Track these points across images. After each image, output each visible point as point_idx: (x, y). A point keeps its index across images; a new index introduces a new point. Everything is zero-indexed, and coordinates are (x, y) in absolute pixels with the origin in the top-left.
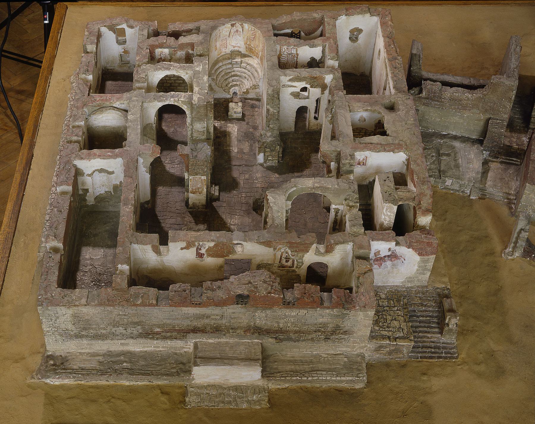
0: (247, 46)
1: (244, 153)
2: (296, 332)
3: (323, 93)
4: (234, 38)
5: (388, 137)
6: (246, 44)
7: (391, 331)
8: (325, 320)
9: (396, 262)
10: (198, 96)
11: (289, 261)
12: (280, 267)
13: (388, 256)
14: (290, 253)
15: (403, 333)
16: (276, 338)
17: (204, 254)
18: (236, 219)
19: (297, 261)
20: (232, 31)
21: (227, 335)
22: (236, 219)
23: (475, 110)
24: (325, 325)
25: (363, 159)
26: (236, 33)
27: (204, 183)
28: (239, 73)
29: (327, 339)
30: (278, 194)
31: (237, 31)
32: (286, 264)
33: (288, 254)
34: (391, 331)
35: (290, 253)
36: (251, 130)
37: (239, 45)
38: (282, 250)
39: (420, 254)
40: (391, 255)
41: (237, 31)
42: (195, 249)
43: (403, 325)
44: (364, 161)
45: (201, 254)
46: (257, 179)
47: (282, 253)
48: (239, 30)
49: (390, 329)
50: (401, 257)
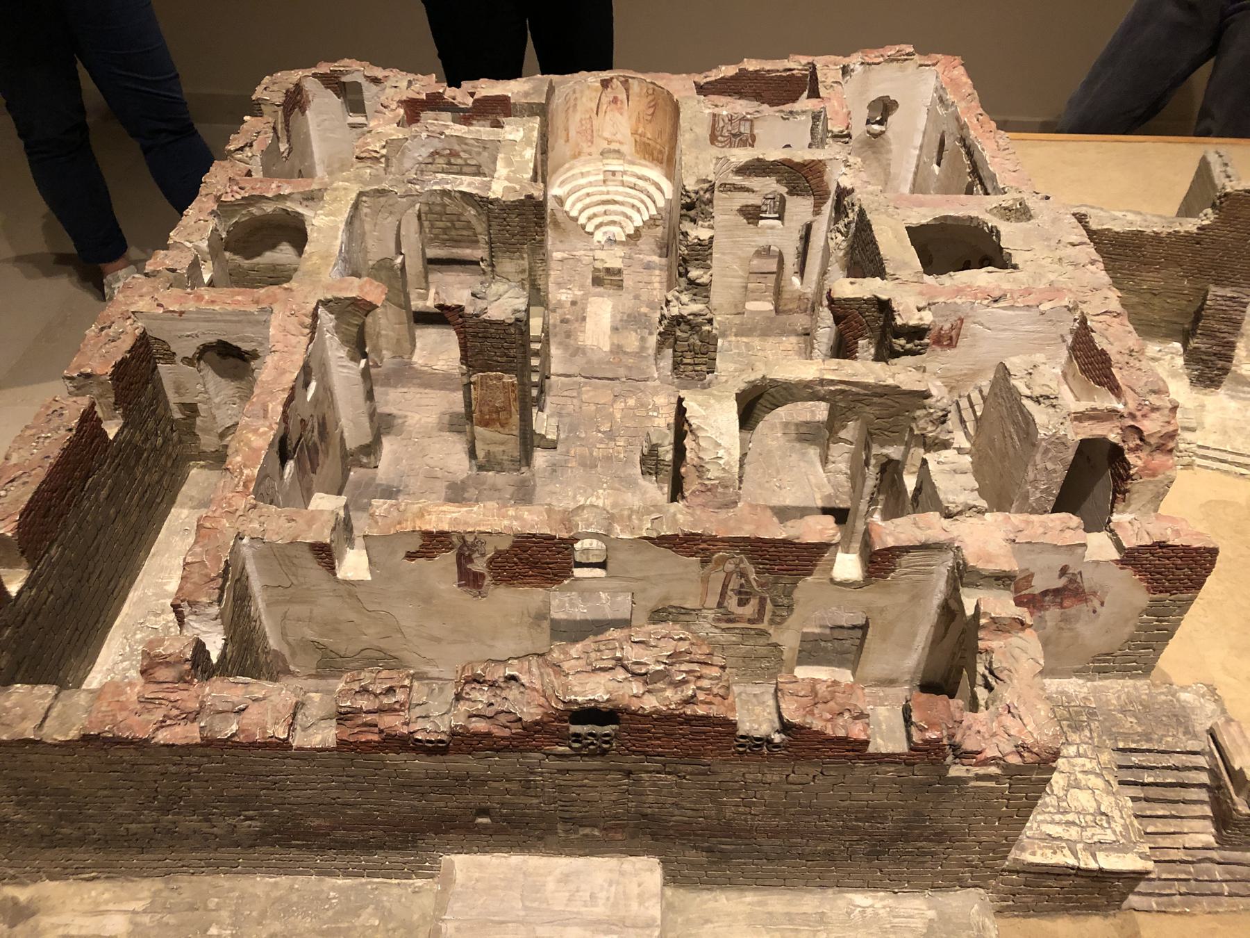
0: (638, 138)
1: (625, 353)
2: (774, 833)
3: (817, 212)
4: (607, 117)
5: (1017, 274)
6: (634, 133)
7: (1073, 823)
8: (877, 797)
9: (1073, 611)
10: (506, 184)
11: (748, 601)
12: (719, 620)
13: (1056, 592)
14: (753, 576)
15: (1114, 832)
16: (710, 850)
17: (482, 575)
18: (598, 498)
19: (773, 601)
20: (605, 100)
21: (549, 839)
22: (598, 498)
23: (1173, 270)
24: (873, 814)
25: (952, 328)
26: (613, 106)
27: (512, 396)
28: (618, 198)
29: (875, 853)
30: (713, 395)
31: (615, 100)
32: (740, 611)
33: (748, 581)
34: (1073, 823)
35: (753, 576)
36: (644, 310)
37: (619, 137)
38: (729, 567)
39: (1153, 589)
40: (1064, 588)
41: (615, 100)
42: (451, 556)
43: (1107, 803)
44: (953, 333)
45: (475, 574)
46: (656, 408)
47: (728, 575)
48: (620, 97)
49: (1070, 817)
50: (1094, 594)
